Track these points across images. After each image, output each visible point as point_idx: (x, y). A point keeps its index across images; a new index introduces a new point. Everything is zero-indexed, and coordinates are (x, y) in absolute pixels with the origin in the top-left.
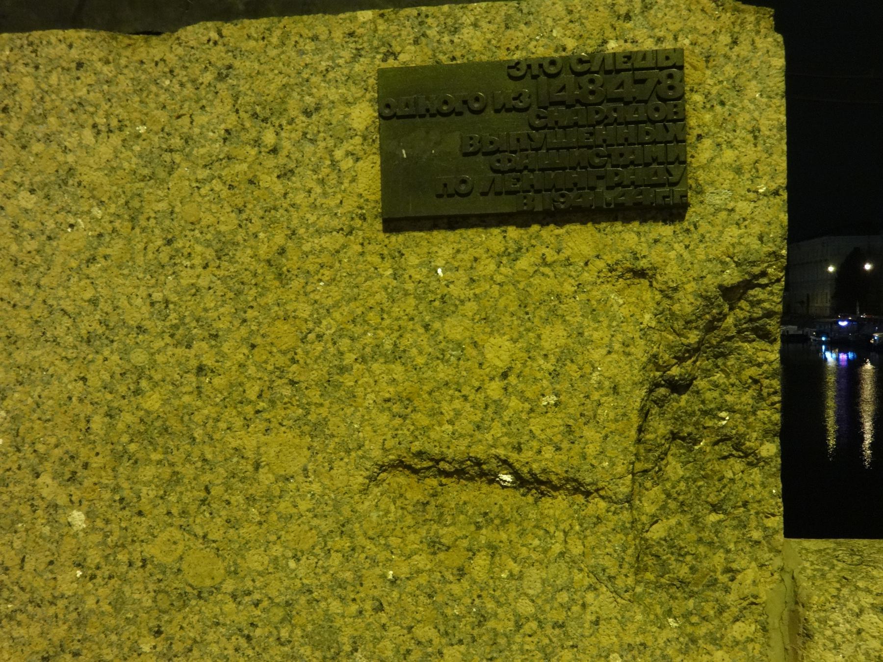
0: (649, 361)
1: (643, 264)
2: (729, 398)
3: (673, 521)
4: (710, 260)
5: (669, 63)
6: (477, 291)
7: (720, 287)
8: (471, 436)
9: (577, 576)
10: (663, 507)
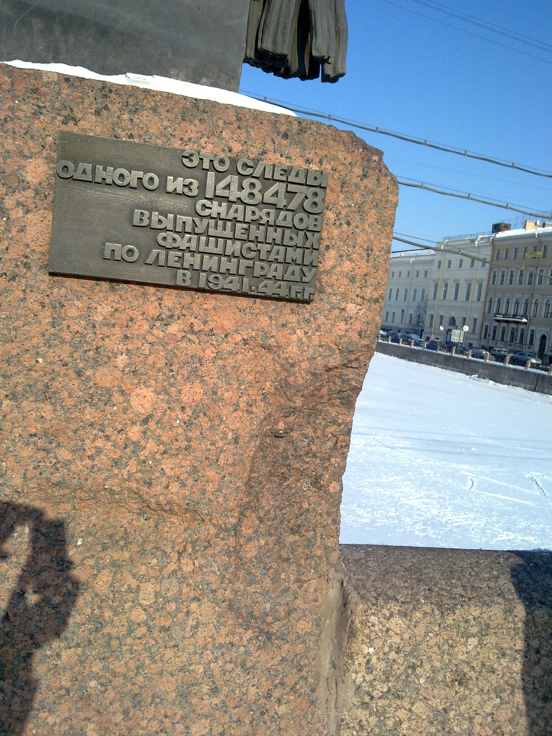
6: (130, 347)
7: (326, 366)
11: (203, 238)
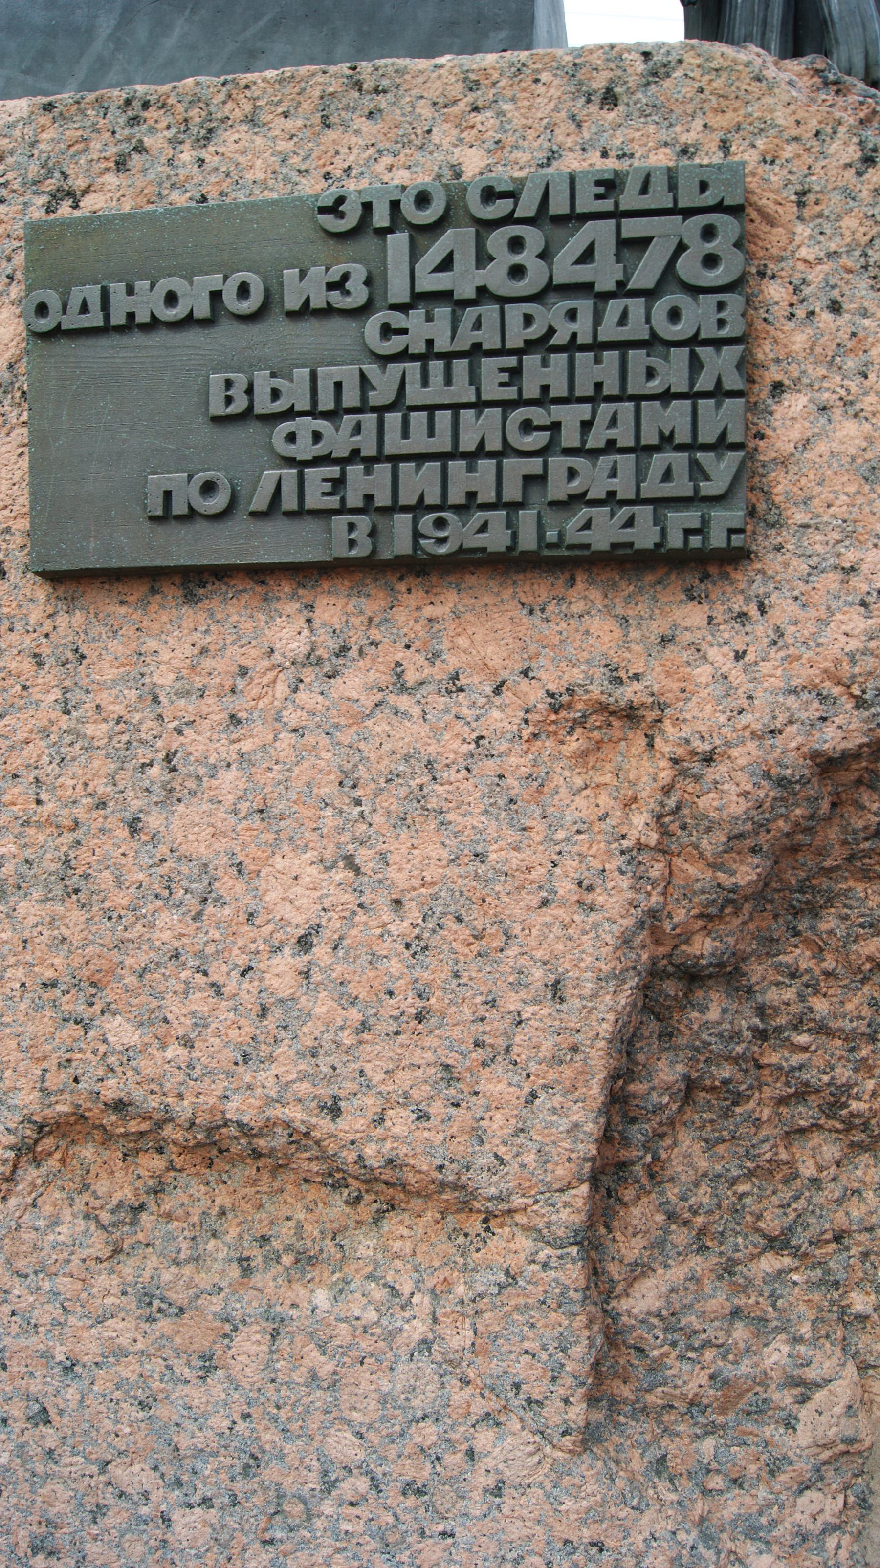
0: (641, 924)
1: (630, 693)
2: (820, 1006)
3: (677, 1273)
4: (794, 692)
5: (709, 198)
6: (246, 746)
7: (815, 755)
8: (229, 1075)
9: (459, 1396)
10: (658, 1245)
11: (393, 419)
